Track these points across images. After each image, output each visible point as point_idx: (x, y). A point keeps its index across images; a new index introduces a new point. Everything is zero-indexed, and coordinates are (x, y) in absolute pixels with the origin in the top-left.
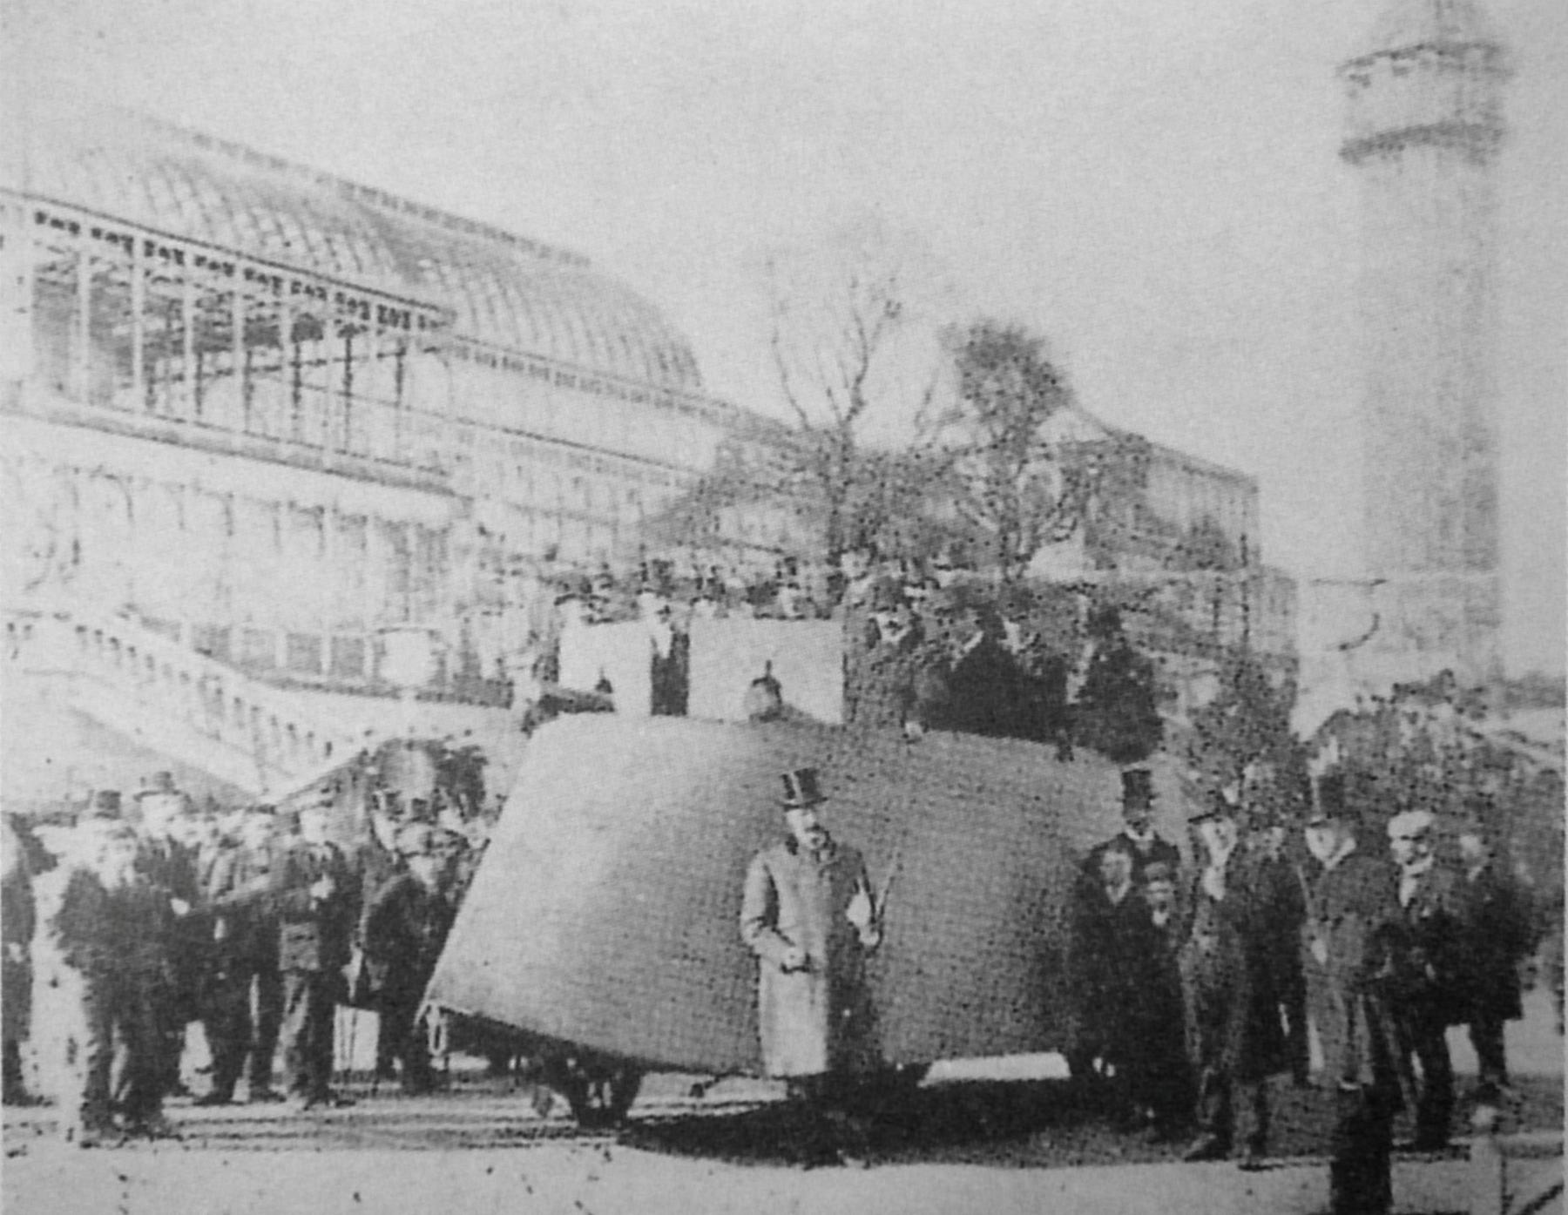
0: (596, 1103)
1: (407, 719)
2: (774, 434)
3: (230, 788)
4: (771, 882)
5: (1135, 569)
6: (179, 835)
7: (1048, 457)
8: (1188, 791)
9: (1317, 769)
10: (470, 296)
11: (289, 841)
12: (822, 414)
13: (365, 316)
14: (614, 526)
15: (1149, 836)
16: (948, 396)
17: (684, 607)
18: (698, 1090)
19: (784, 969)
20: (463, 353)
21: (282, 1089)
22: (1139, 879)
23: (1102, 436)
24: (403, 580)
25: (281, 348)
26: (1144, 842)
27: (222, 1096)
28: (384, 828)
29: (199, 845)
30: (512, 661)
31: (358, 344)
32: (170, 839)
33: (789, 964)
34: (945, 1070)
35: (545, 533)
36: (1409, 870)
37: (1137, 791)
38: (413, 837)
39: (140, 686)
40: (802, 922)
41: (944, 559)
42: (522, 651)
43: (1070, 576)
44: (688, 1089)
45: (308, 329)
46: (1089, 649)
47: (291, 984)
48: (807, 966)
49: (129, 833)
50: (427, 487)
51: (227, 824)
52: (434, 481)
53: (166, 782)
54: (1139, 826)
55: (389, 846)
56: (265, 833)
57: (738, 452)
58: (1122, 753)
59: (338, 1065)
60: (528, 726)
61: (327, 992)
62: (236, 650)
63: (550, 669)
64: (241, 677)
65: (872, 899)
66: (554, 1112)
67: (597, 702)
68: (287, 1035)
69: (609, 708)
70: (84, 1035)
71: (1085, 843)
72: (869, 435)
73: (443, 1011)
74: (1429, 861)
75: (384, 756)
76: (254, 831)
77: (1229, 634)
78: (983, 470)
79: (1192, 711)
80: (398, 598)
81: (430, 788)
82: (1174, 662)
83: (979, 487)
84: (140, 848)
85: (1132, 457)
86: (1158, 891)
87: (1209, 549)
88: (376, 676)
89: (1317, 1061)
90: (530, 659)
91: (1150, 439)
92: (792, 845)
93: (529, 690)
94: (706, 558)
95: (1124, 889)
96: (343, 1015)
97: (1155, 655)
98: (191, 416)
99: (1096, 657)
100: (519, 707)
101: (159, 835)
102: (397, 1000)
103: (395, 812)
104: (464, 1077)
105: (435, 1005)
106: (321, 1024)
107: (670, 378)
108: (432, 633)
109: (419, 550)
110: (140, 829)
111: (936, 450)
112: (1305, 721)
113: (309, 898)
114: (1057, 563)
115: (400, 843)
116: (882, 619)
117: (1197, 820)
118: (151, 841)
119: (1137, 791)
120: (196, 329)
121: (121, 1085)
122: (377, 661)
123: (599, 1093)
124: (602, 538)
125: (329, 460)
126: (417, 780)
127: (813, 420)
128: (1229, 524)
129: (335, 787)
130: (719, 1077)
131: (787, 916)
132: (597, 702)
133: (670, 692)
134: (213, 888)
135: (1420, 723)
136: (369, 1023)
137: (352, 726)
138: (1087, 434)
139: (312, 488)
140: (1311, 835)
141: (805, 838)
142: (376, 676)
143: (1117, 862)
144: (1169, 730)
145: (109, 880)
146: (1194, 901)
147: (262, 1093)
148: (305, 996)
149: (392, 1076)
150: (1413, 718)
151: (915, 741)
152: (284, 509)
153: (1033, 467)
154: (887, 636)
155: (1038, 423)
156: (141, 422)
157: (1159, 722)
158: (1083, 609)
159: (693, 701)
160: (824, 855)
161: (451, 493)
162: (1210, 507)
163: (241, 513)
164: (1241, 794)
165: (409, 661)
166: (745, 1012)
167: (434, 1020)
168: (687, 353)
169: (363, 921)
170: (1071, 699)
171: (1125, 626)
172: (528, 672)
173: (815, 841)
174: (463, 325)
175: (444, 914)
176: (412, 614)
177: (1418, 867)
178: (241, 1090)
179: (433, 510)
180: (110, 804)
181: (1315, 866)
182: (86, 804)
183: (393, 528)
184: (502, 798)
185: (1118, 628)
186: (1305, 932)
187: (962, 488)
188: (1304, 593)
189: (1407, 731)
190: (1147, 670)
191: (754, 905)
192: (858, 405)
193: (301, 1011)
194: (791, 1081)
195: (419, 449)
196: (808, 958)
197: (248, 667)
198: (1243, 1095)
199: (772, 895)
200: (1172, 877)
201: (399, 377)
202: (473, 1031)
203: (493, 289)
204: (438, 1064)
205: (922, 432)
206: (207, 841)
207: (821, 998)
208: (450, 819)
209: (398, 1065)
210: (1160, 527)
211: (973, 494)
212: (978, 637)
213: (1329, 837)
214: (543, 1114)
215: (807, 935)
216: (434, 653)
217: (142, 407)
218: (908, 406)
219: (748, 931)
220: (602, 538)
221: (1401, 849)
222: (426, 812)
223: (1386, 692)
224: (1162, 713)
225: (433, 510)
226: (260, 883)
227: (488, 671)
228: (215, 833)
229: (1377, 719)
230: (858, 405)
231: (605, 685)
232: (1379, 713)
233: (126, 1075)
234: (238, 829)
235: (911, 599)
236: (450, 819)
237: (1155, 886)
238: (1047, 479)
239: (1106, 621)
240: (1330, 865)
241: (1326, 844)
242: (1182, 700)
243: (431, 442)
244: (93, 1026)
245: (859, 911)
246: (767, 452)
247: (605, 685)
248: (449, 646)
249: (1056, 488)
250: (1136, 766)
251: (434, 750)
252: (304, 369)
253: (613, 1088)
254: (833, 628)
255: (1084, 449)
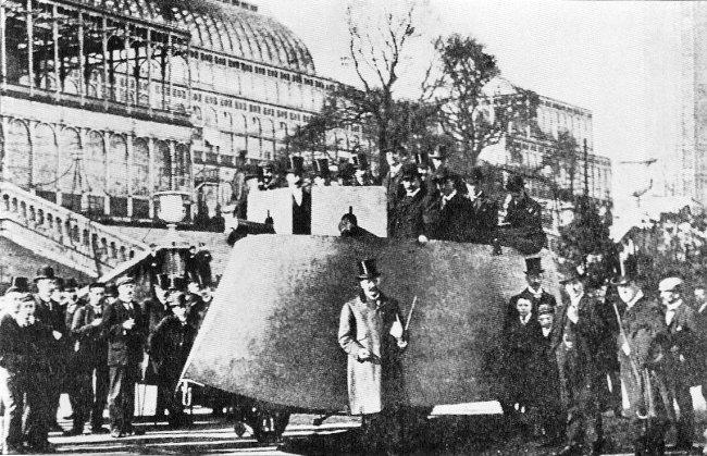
0: (267, 429)
1: (168, 239)
2: (348, 92)
3: (81, 275)
4: (352, 313)
5: (532, 158)
6: (57, 299)
7: (488, 102)
8: (560, 269)
9: (623, 257)
10: (198, 26)
11: (112, 300)
12: (375, 83)
13: (145, 37)
14: (273, 141)
15: (540, 291)
16: (438, 73)
17: (307, 180)
18: (318, 422)
19: (359, 360)
20: (195, 55)
21: (108, 426)
22: (535, 312)
23: (515, 92)
24: (167, 171)
25: (102, 53)
26: (538, 295)
27: (77, 430)
28: (160, 293)
29: (67, 304)
30: (225, 208)
31: (142, 52)
32: (51, 300)
33: (362, 357)
34: (440, 410)
35: (239, 143)
36: (670, 307)
37: (534, 268)
38: (175, 297)
39: (36, 225)
40: (368, 335)
41: (436, 154)
42: (228, 204)
43: (502, 162)
44: (312, 422)
45: (116, 44)
46: (509, 198)
47: (113, 372)
48: (371, 358)
49: (32, 298)
50: (176, 123)
51: (80, 293)
52: (181, 120)
53: (49, 273)
54: (536, 286)
55: (164, 302)
56: (99, 297)
57: (334, 103)
58: (524, 251)
59: (136, 414)
60: (232, 240)
61: (131, 378)
62: (84, 206)
63: (241, 211)
64: (86, 220)
65: (403, 324)
66: (245, 435)
67: (267, 227)
68: (111, 398)
69: (272, 231)
70: (8, 402)
71: (508, 294)
72: (399, 93)
73: (190, 385)
74: (680, 301)
75: (163, 254)
76: (94, 295)
77: (578, 192)
78: (456, 110)
79: (560, 229)
80: (166, 179)
81: (183, 273)
82: (551, 204)
83: (454, 118)
84: (37, 306)
85: (527, 102)
86: (545, 319)
87: (565, 150)
88: (156, 217)
89: (626, 404)
90: (232, 207)
91: (497, 64)
92: (364, 298)
93: (231, 223)
94: (319, 155)
95: (528, 318)
96: (139, 389)
97: (541, 201)
98: (60, 90)
99: (512, 201)
100: (228, 231)
101: (47, 300)
102: (165, 379)
103: (165, 285)
104: (201, 417)
105: (186, 381)
106: (128, 391)
107: (297, 64)
108: (183, 196)
109: (175, 159)
110: (36, 296)
111: (432, 100)
112: (616, 233)
113: (123, 329)
114: (494, 154)
115: (169, 300)
116: (407, 184)
117: (564, 283)
118: (43, 302)
119: (534, 268)
120: (27, 36)
121: (26, 429)
122: (155, 209)
123: (268, 425)
124: (268, 146)
125: (83, 102)
126: (177, 271)
127: (371, 87)
128: (578, 133)
129: (135, 273)
130: (329, 415)
131: (361, 334)
132: (267, 227)
133: (302, 221)
134: (74, 325)
135: (675, 232)
136: (152, 391)
137: (142, 242)
138: (510, 91)
139: (121, 124)
140: (621, 290)
141: (369, 295)
142: (156, 217)
143: (524, 306)
144: (549, 238)
145: (21, 322)
146: (563, 324)
147: (97, 429)
148: (121, 376)
149: (165, 418)
150: (670, 230)
151: (423, 245)
152: (107, 135)
153: (480, 108)
154: (410, 193)
155: (482, 86)
156: (33, 92)
157: (544, 235)
158: (506, 179)
159: (314, 229)
160: (378, 303)
161: (191, 126)
162: (569, 128)
163: (85, 139)
164: (586, 269)
165: (171, 209)
166: (340, 384)
167: (185, 389)
168: (308, 54)
169: (149, 339)
170: (500, 224)
171: (526, 186)
172: (231, 215)
173: (374, 296)
174: (195, 40)
175: (190, 331)
176: (173, 187)
177: (675, 305)
178: (87, 427)
179: (181, 134)
180: (22, 285)
181: (623, 306)
182: (9, 285)
183: (163, 144)
184: (219, 278)
185: (523, 186)
186: (619, 339)
187: (445, 119)
188: (615, 167)
189: (667, 237)
190: (538, 207)
191: (344, 328)
192: (393, 78)
193: (118, 385)
194: (365, 417)
195: (175, 101)
196: (372, 354)
197: (90, 214)
198: (591, 420)
199: (353, 321)
200: (552, 311)
201: (163, 65)
202: (201, 394)
203: (209, 22)
204: (188, 411)
205: (425, 91)
206: (71, 302)
207: (378, 376)
208: (193, 288)
209: (167, 412)
210: (541, 136)
211: (451, 122)
212: (454, 192)
213: (629, 290)
214: (240, 437)
215: (371, 343)
216: (184, 205)
217: (33, 85)
218: (417, 78)
219: (341, 342)
220: (268, 146)
221: (666, 296)
222: (181, 284)
223: (658, 219)
224: (545, 230)
225: (181, 134)
226: (97, 322)
227: (212, 214)
228: (75, 297)
229: (654, 230)
230: (393, 78)
231: (270, 220)
232: (654, 227)
233: (29, 421)
234: (87, 295)
235: (421, 174)
236: (193, 288)
237: (543, 316)
238: (487, 113)
239: (516, 184)
240: (631, 305)
241: (629, 295)
242: (555, 224)
243: (180, 100)
244: (13, 396)
245: (396, 330)
246: (348, 103)
247: (270, 220)
248: (193, 202)
249: (491, 119)
250: (533, 256)
251: (184, 253)
252: (115, 64)
253: (275, 421)
254: (383, 189)
255: (505, 98)
